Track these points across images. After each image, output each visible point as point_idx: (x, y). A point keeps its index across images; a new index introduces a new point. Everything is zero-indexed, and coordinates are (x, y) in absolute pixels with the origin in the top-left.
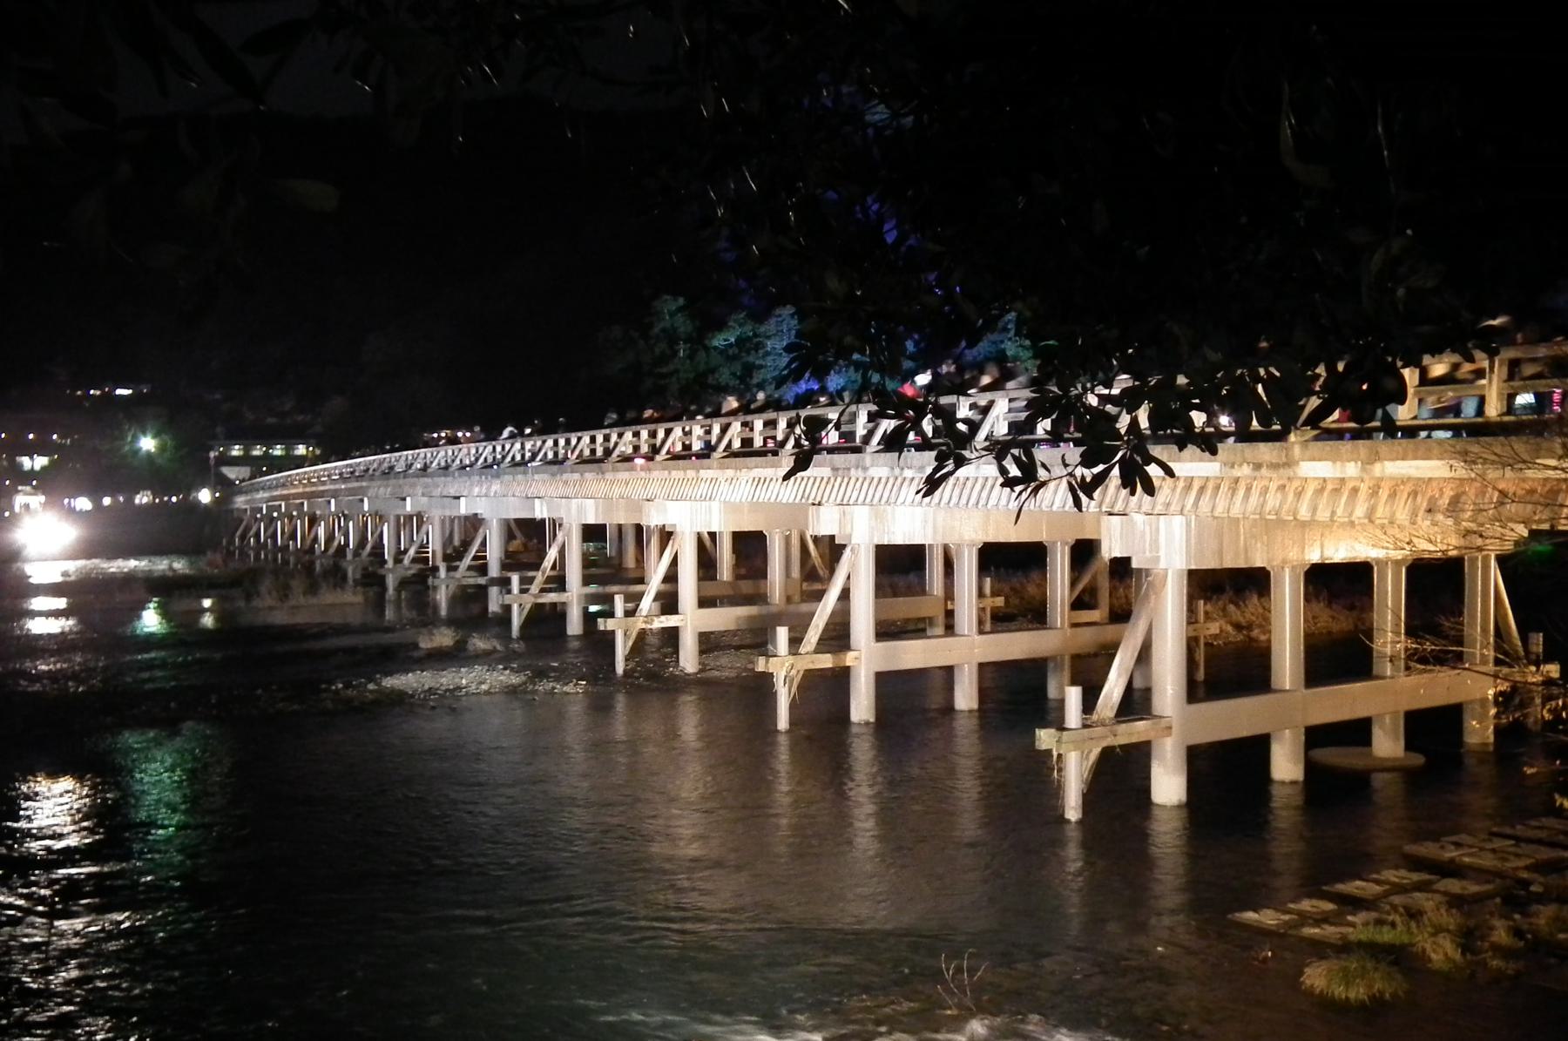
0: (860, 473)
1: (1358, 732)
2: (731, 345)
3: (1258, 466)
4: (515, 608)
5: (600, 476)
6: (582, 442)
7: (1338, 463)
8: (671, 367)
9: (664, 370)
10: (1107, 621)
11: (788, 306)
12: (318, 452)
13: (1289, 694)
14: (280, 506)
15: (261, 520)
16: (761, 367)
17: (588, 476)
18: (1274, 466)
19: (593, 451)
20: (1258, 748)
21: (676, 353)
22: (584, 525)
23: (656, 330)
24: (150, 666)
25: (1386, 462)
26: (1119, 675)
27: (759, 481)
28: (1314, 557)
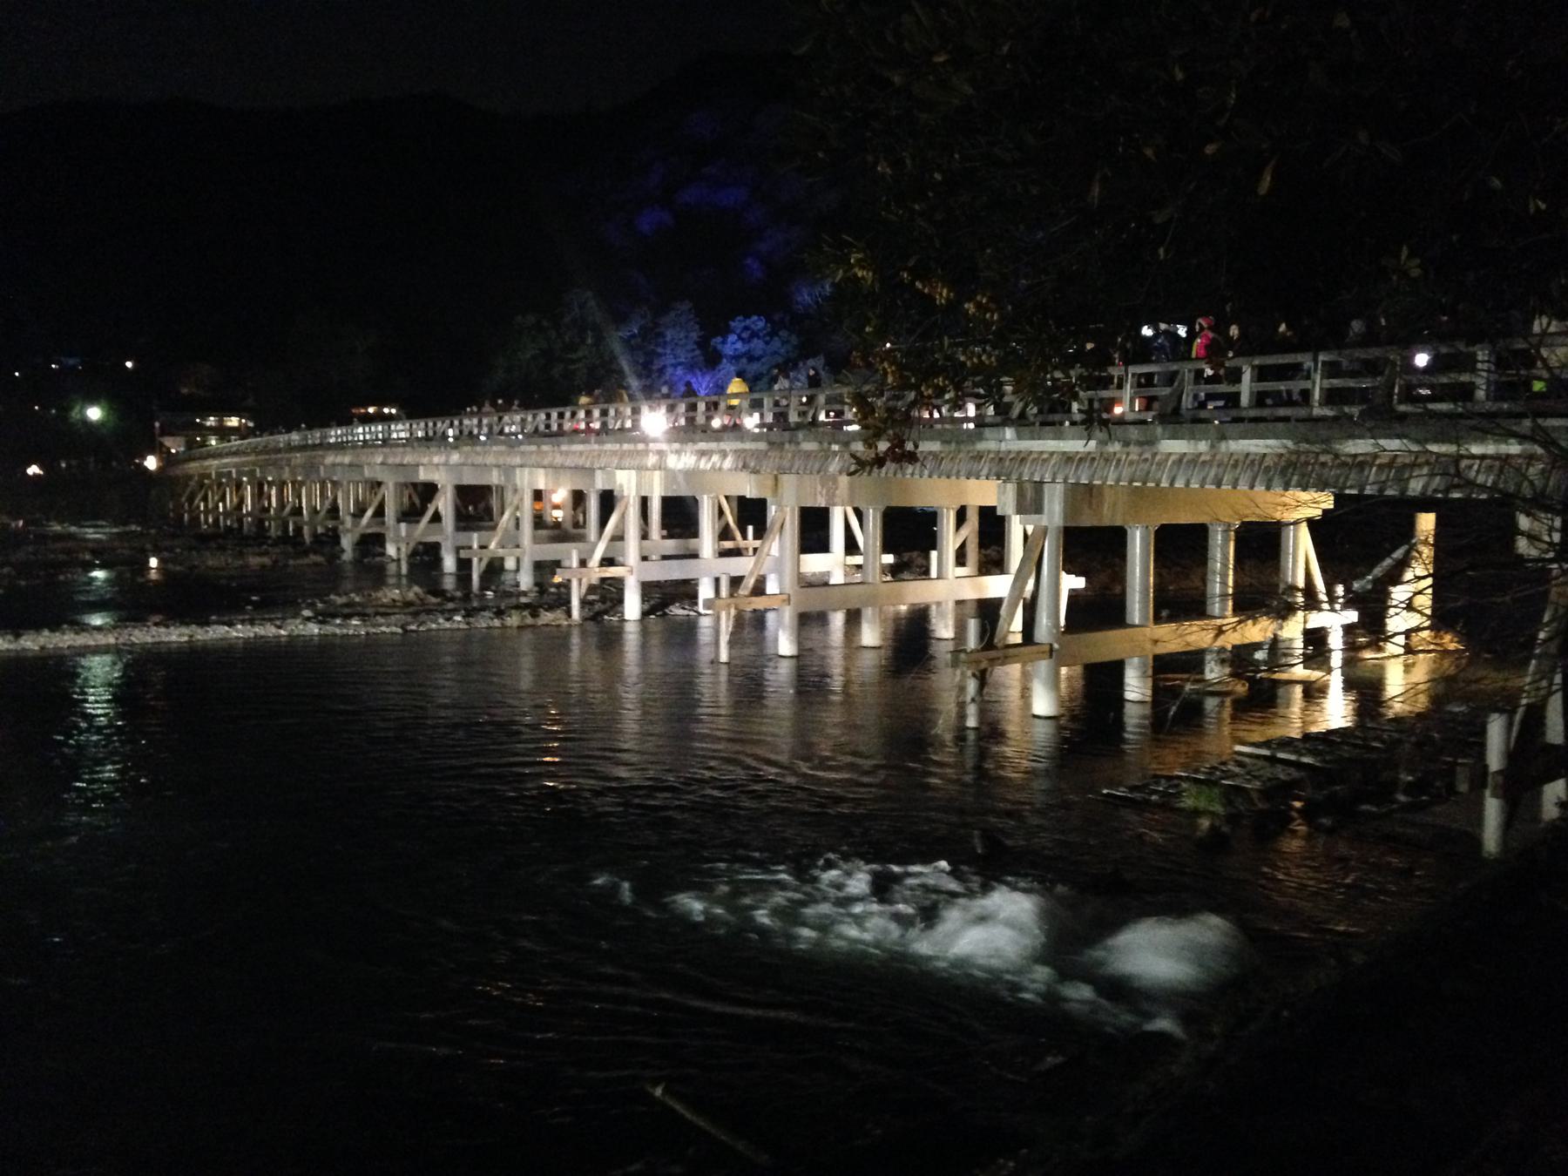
0: (793, 447)
1: (1191, 661)
2: (634, 336)
3: (1126, 444)
4: (475, 560)
5: (556, 448)
6: (538, 419)
7: (1192, 442)
8: (580, 354)
9: (574, 356)
10: (977, 573)
11: (687, 302)
12: (251, 424)
13: (1138, 629)
14: (230, 472)
15: (210, 487)
16: (660, 355)
17: (545, 448)
18: (1140, 444)
19: (548, 426)
20: (1114, 671)
21: (583, 341)
22: (981, 507)
23: (567, 319)
24: (1291, 887)
25: (1231, 442)
26: (606, 571)
27: (702, 453)
28: (1166, 520)
